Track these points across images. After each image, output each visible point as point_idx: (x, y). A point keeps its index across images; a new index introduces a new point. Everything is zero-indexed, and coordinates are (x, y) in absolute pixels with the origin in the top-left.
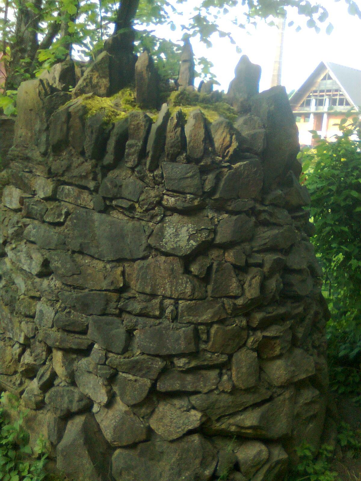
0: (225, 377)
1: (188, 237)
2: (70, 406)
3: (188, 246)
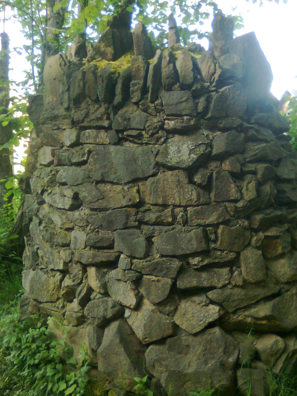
0: (236, 273)
1: (189, 152)
2: (106, 313)
3: (190, 159)
